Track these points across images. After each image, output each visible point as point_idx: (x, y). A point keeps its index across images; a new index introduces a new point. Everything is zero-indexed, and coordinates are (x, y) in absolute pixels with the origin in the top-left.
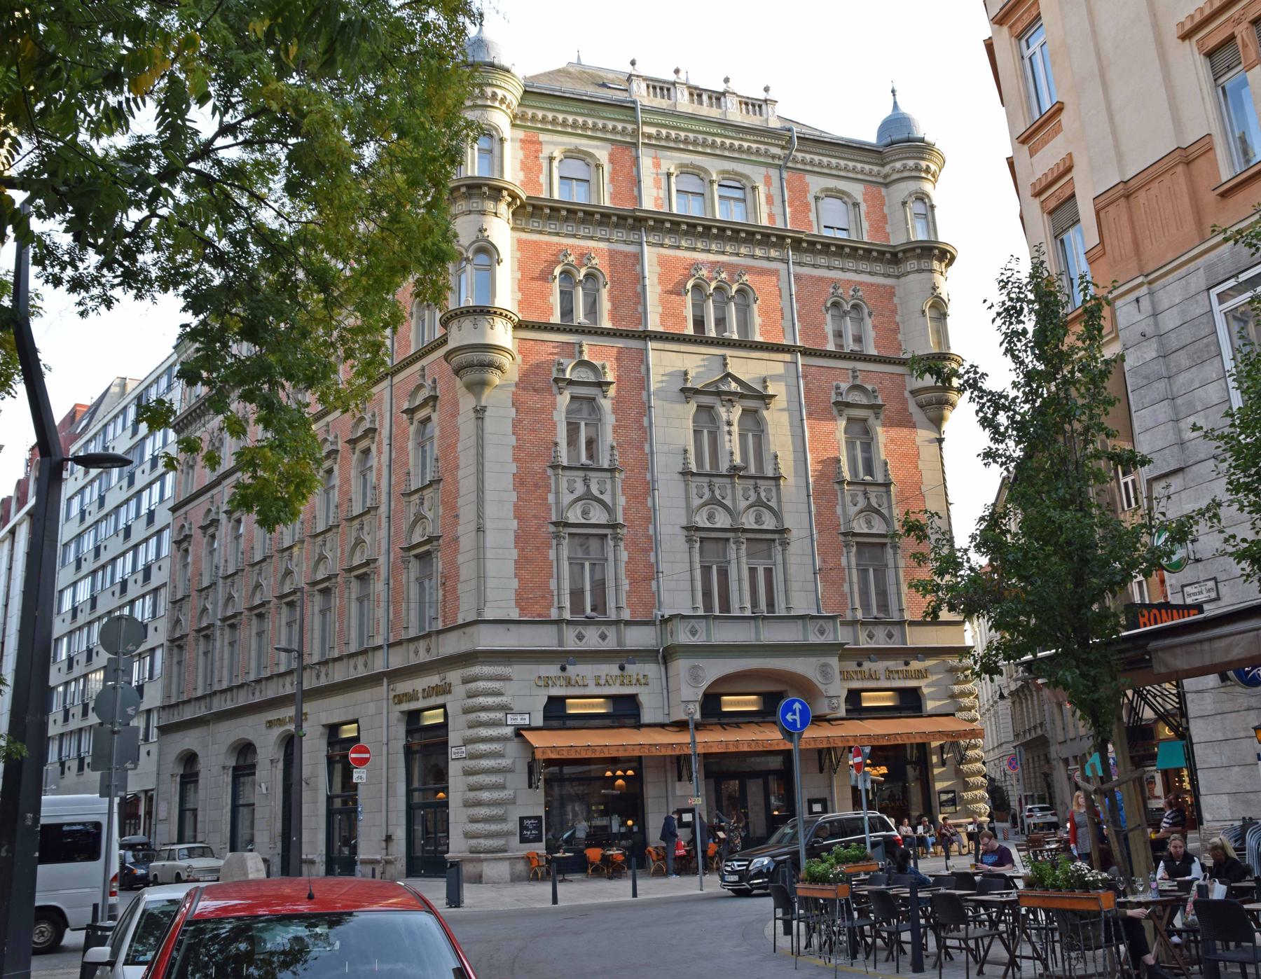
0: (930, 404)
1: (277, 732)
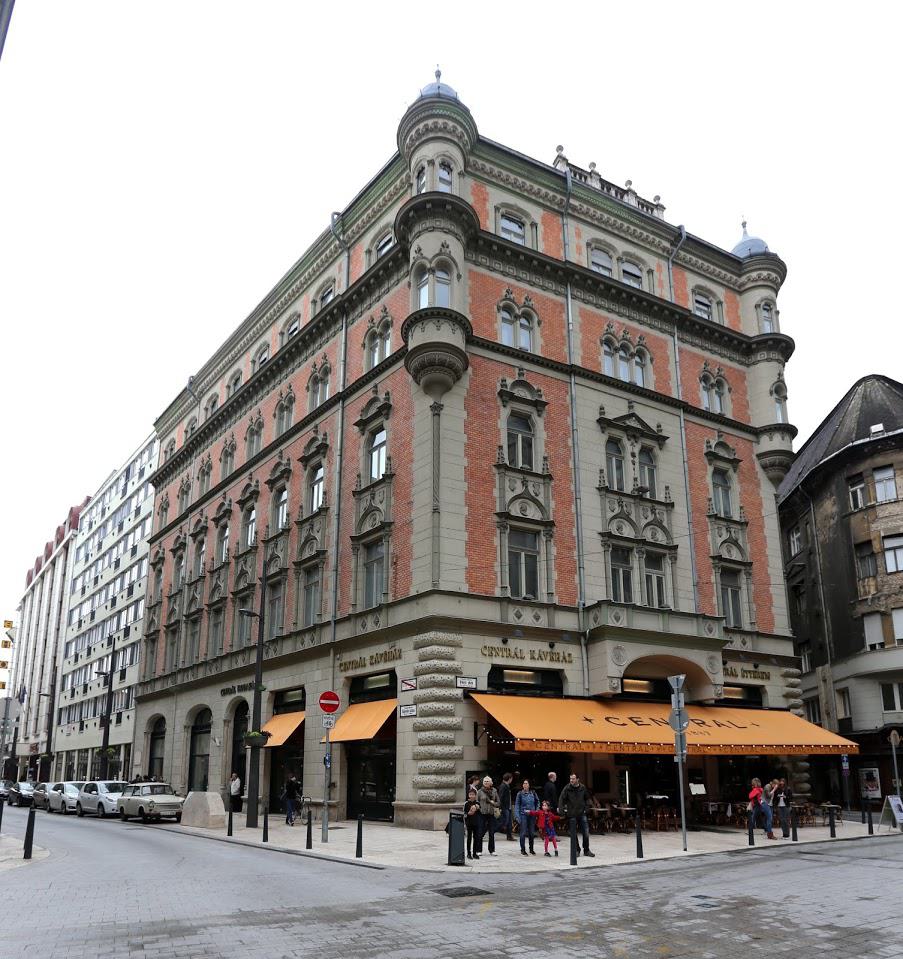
0: (773, 465)
1: (229, 698)
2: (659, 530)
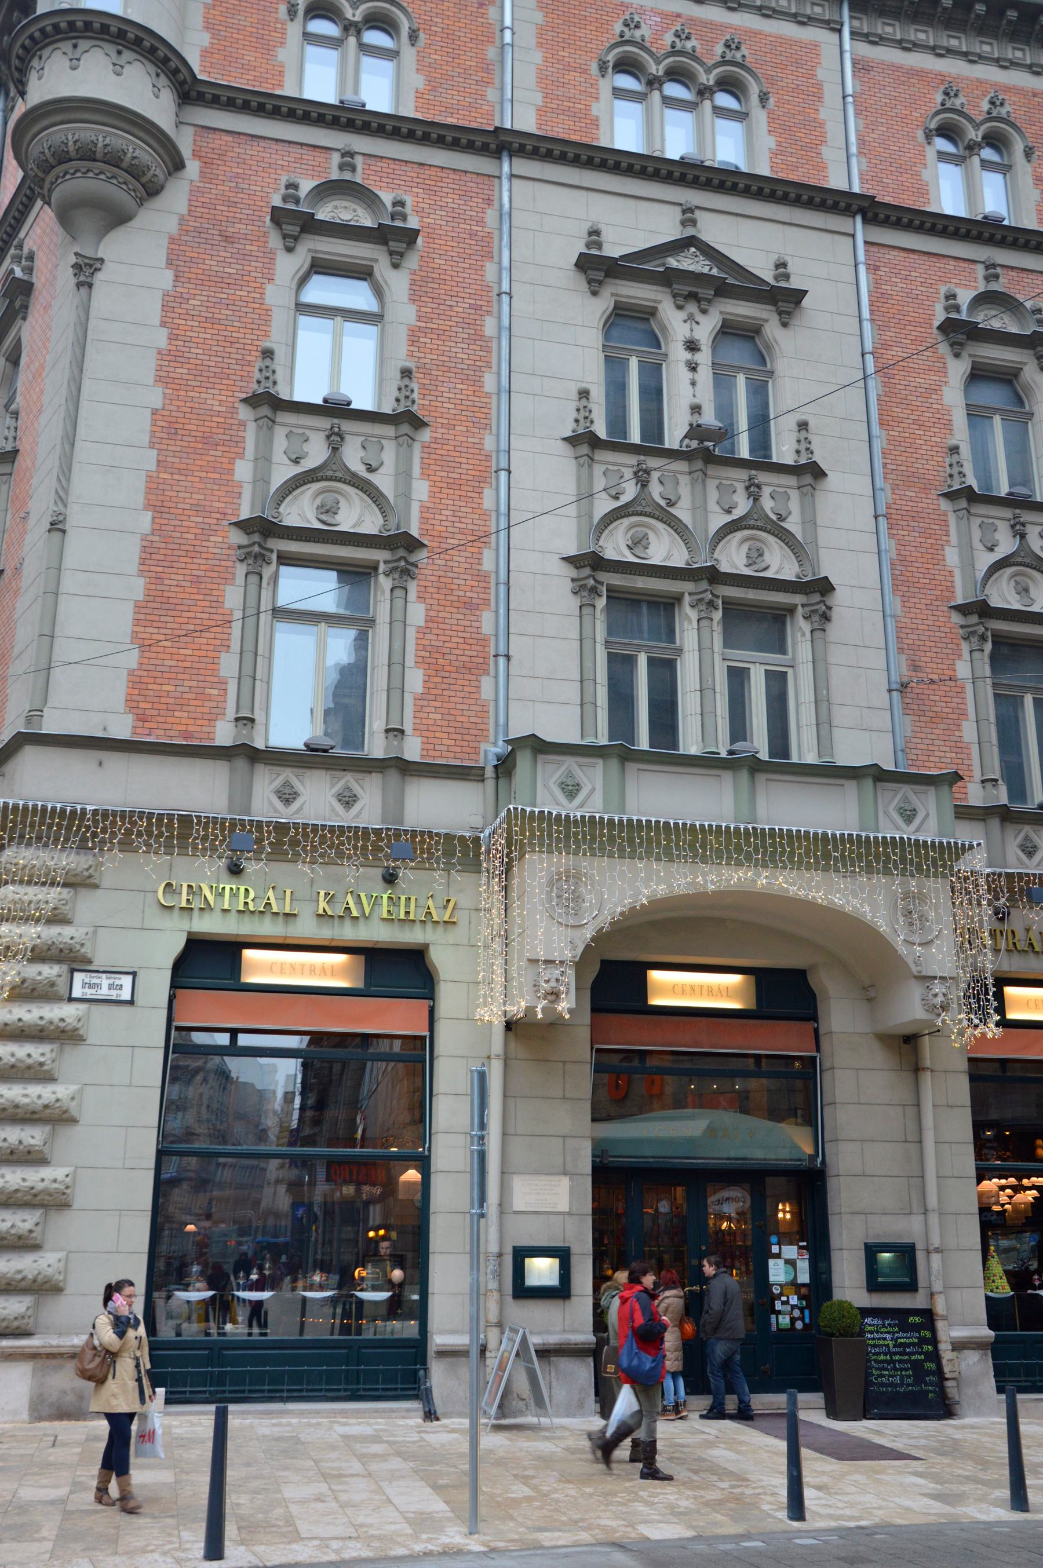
2: (771, 539)
